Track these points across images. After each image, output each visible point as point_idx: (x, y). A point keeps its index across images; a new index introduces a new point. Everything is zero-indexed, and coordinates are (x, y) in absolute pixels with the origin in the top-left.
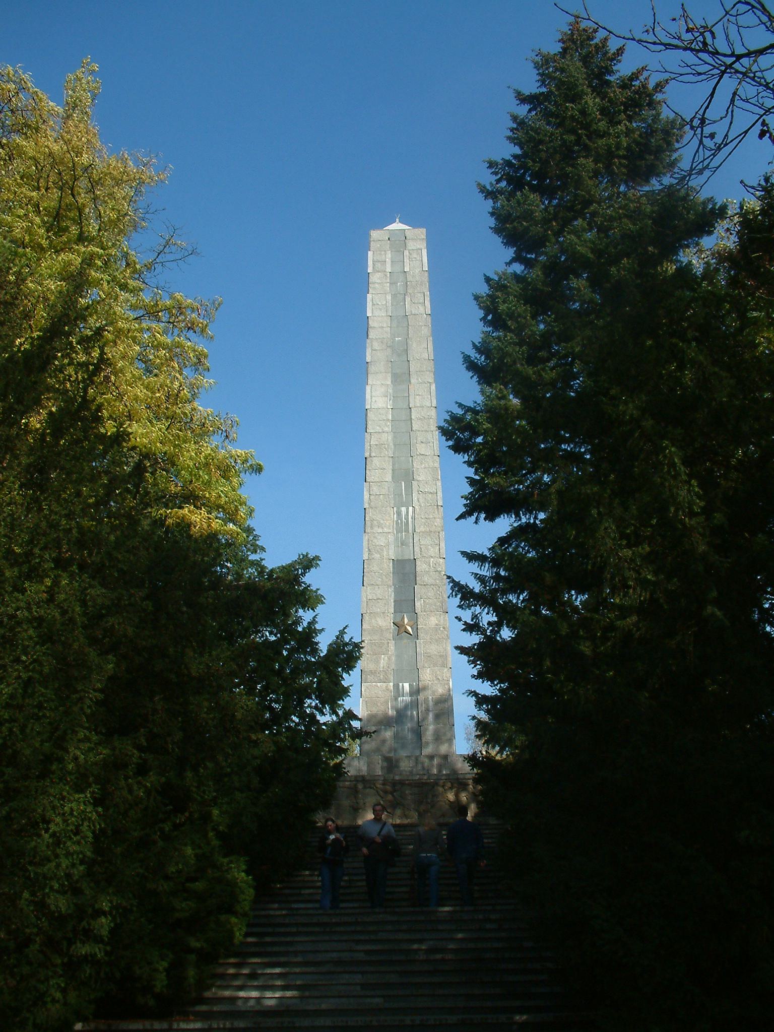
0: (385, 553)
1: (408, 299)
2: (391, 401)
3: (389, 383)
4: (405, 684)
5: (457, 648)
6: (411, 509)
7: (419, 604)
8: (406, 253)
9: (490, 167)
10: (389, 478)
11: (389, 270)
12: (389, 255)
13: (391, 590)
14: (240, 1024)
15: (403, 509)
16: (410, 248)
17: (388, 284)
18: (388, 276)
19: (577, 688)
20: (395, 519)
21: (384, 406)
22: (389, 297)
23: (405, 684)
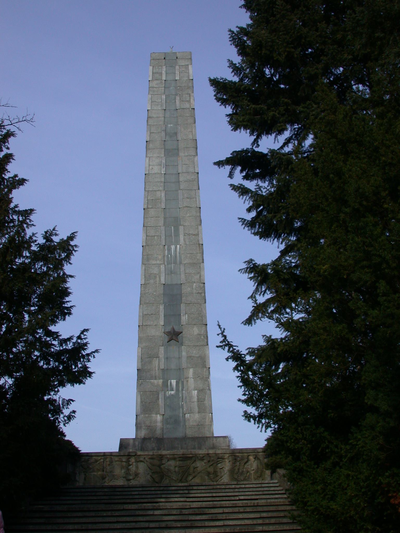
0: (158, 279)
1: (178, 98)
2: (164, 169)
3: (163, 155)
4: (172, 381)
5: (215, 164)
6: (178, 246)
7: (184, 318)
8: (177, 67)
9: (231, 187)
10: (161, 223)
11: (164, 78)
12: (164, 69)
13: (211, 529)
14: (228, 530)
15: (173, 247)
16: (180, 64)
17: (163, 88)
18: (164, 82)
19: (380, 294)
20: (166, 254)
21: (159, 172)
22: (164, 97)
23: (172, 381)
